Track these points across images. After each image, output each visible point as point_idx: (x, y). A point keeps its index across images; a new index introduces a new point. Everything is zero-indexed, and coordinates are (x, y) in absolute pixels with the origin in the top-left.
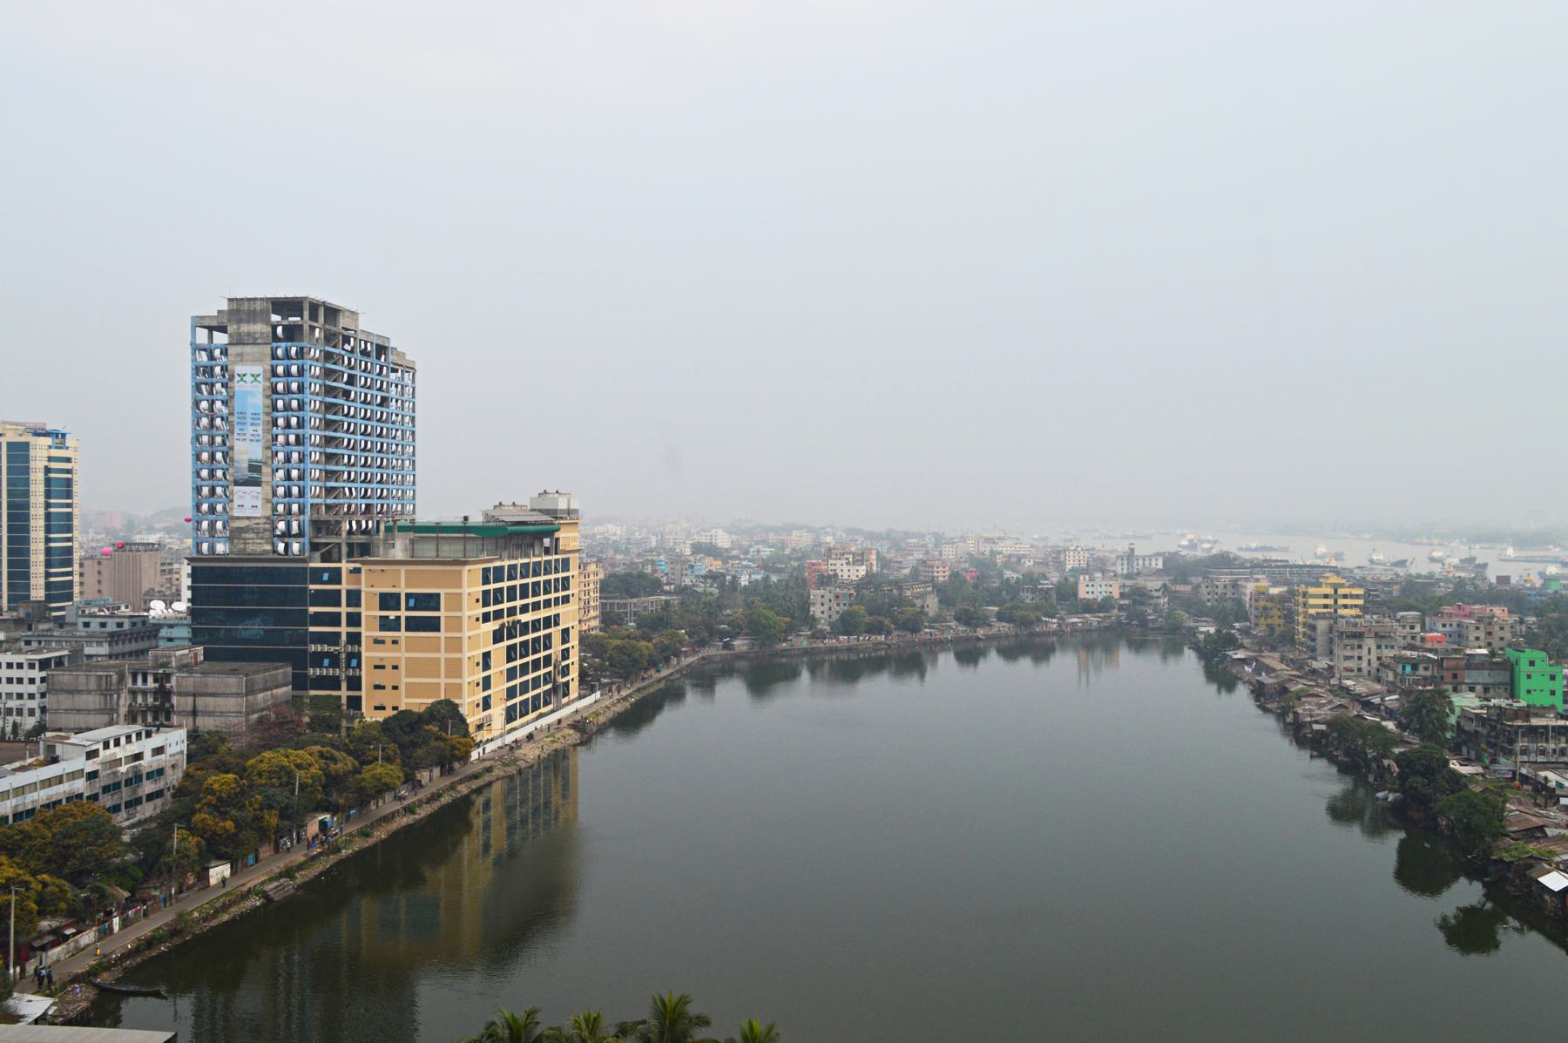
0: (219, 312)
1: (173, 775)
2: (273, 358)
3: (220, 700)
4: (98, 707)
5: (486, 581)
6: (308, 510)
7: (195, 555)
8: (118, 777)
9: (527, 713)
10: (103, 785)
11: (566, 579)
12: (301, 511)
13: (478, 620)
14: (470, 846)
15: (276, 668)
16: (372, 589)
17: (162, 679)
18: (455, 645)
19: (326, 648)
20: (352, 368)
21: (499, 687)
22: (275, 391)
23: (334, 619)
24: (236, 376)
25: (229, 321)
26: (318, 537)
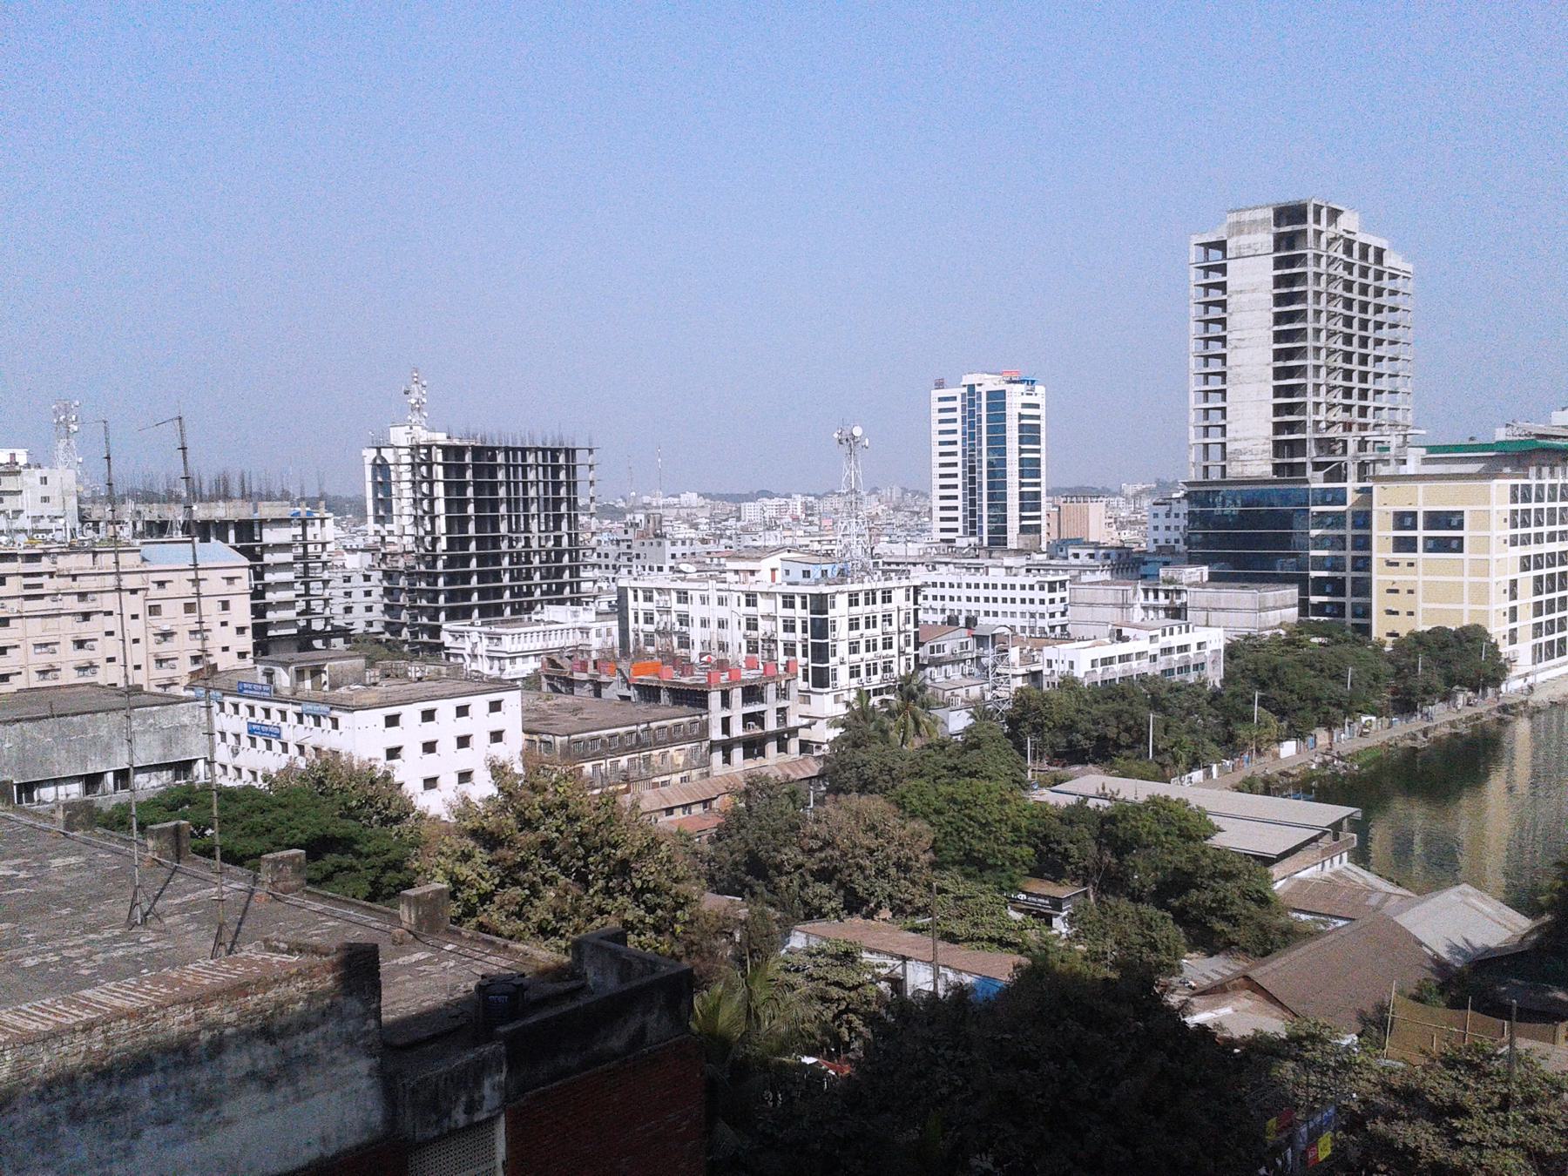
5: (1514, 500)
13: (1505, 542)
14: (1496, 785)
16: (1385, 508)
18: (1483, 568)
21: (1526, 621)
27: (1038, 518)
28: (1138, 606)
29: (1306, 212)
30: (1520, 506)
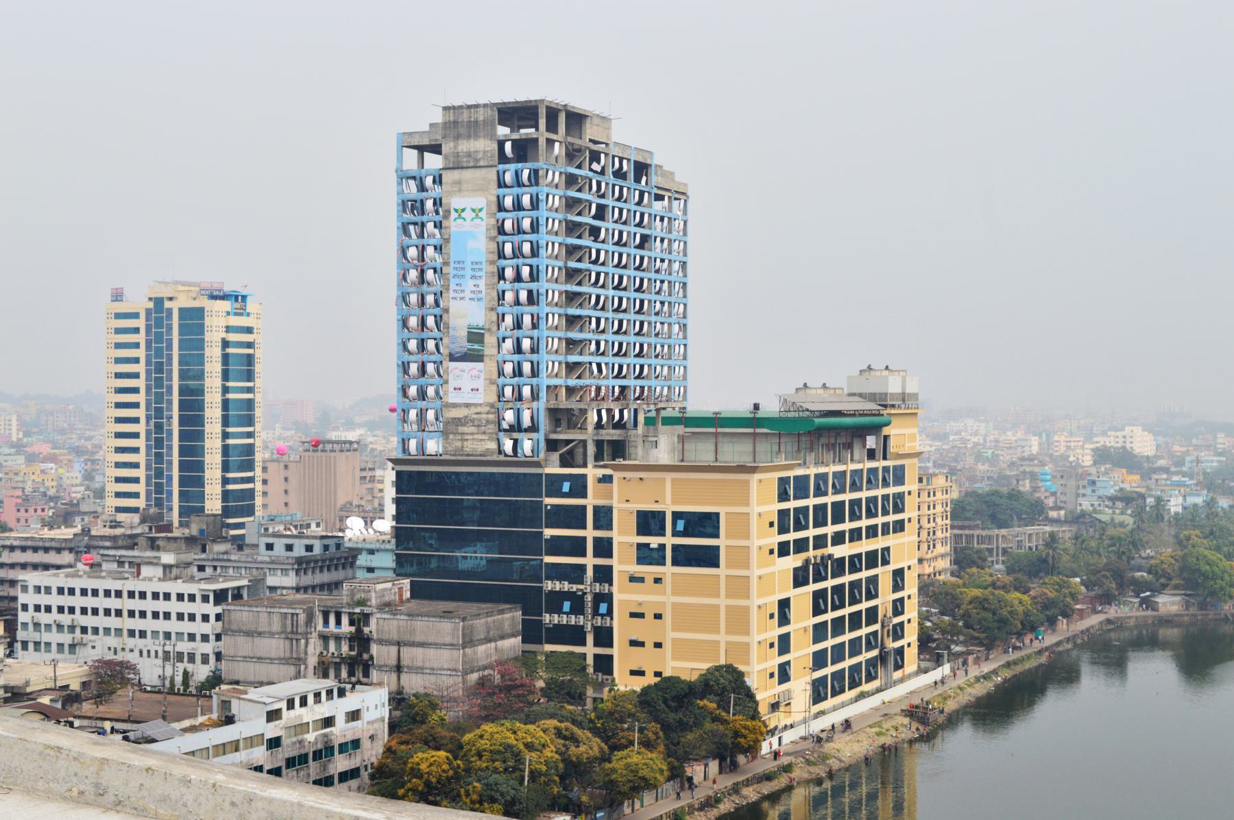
0: (431, 125)
1: (372, 749)
2: (500, 186)
3: (431, 652)
4: (282, 655)
5: (783, 496)
6: (543, 394)
7: (400, 456)
8: (304, 747)
9: (842, 691)
10: (287, 756)
11: (900, 497)
12: (535, 396)
13: (771, 552)
15: (502, 612)
17: (359, 620)
18: (740, 587)
19: (566, 586)
20: (603, 196)
22: (501, 230)
23: (577, 547)
24: (452, 211)
25: (444, 137)
26: (555, 432)
27: (251, 480)
28: (315, 635)
29: (537, 114)
30: (792, 504)
